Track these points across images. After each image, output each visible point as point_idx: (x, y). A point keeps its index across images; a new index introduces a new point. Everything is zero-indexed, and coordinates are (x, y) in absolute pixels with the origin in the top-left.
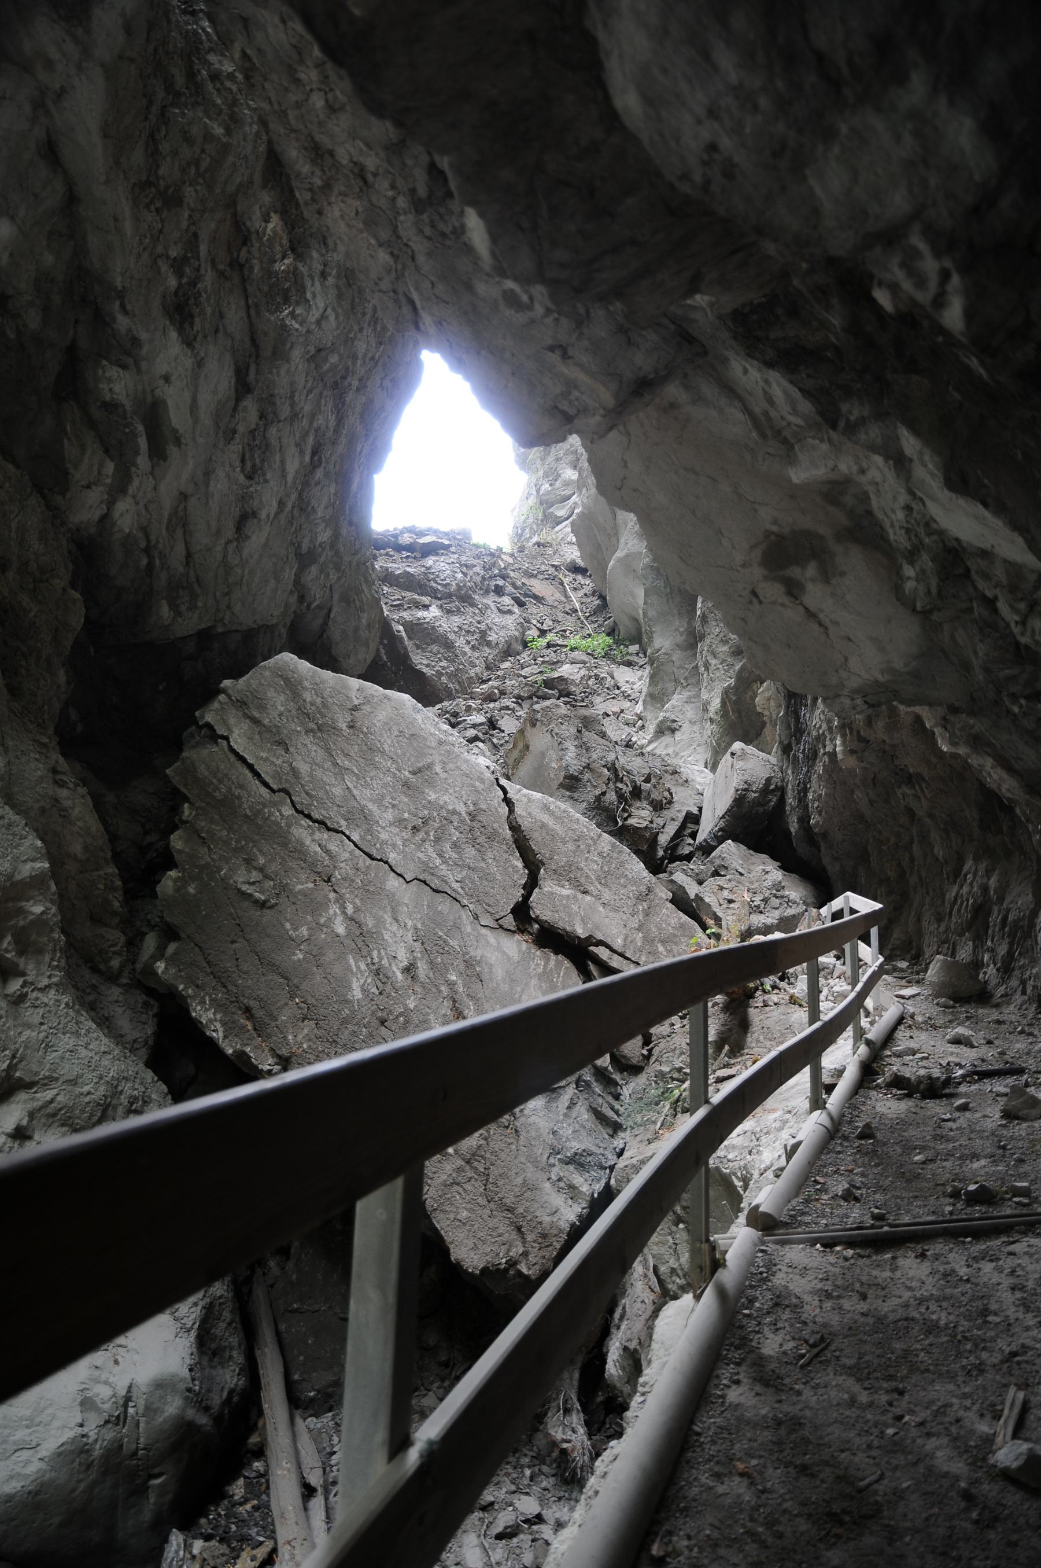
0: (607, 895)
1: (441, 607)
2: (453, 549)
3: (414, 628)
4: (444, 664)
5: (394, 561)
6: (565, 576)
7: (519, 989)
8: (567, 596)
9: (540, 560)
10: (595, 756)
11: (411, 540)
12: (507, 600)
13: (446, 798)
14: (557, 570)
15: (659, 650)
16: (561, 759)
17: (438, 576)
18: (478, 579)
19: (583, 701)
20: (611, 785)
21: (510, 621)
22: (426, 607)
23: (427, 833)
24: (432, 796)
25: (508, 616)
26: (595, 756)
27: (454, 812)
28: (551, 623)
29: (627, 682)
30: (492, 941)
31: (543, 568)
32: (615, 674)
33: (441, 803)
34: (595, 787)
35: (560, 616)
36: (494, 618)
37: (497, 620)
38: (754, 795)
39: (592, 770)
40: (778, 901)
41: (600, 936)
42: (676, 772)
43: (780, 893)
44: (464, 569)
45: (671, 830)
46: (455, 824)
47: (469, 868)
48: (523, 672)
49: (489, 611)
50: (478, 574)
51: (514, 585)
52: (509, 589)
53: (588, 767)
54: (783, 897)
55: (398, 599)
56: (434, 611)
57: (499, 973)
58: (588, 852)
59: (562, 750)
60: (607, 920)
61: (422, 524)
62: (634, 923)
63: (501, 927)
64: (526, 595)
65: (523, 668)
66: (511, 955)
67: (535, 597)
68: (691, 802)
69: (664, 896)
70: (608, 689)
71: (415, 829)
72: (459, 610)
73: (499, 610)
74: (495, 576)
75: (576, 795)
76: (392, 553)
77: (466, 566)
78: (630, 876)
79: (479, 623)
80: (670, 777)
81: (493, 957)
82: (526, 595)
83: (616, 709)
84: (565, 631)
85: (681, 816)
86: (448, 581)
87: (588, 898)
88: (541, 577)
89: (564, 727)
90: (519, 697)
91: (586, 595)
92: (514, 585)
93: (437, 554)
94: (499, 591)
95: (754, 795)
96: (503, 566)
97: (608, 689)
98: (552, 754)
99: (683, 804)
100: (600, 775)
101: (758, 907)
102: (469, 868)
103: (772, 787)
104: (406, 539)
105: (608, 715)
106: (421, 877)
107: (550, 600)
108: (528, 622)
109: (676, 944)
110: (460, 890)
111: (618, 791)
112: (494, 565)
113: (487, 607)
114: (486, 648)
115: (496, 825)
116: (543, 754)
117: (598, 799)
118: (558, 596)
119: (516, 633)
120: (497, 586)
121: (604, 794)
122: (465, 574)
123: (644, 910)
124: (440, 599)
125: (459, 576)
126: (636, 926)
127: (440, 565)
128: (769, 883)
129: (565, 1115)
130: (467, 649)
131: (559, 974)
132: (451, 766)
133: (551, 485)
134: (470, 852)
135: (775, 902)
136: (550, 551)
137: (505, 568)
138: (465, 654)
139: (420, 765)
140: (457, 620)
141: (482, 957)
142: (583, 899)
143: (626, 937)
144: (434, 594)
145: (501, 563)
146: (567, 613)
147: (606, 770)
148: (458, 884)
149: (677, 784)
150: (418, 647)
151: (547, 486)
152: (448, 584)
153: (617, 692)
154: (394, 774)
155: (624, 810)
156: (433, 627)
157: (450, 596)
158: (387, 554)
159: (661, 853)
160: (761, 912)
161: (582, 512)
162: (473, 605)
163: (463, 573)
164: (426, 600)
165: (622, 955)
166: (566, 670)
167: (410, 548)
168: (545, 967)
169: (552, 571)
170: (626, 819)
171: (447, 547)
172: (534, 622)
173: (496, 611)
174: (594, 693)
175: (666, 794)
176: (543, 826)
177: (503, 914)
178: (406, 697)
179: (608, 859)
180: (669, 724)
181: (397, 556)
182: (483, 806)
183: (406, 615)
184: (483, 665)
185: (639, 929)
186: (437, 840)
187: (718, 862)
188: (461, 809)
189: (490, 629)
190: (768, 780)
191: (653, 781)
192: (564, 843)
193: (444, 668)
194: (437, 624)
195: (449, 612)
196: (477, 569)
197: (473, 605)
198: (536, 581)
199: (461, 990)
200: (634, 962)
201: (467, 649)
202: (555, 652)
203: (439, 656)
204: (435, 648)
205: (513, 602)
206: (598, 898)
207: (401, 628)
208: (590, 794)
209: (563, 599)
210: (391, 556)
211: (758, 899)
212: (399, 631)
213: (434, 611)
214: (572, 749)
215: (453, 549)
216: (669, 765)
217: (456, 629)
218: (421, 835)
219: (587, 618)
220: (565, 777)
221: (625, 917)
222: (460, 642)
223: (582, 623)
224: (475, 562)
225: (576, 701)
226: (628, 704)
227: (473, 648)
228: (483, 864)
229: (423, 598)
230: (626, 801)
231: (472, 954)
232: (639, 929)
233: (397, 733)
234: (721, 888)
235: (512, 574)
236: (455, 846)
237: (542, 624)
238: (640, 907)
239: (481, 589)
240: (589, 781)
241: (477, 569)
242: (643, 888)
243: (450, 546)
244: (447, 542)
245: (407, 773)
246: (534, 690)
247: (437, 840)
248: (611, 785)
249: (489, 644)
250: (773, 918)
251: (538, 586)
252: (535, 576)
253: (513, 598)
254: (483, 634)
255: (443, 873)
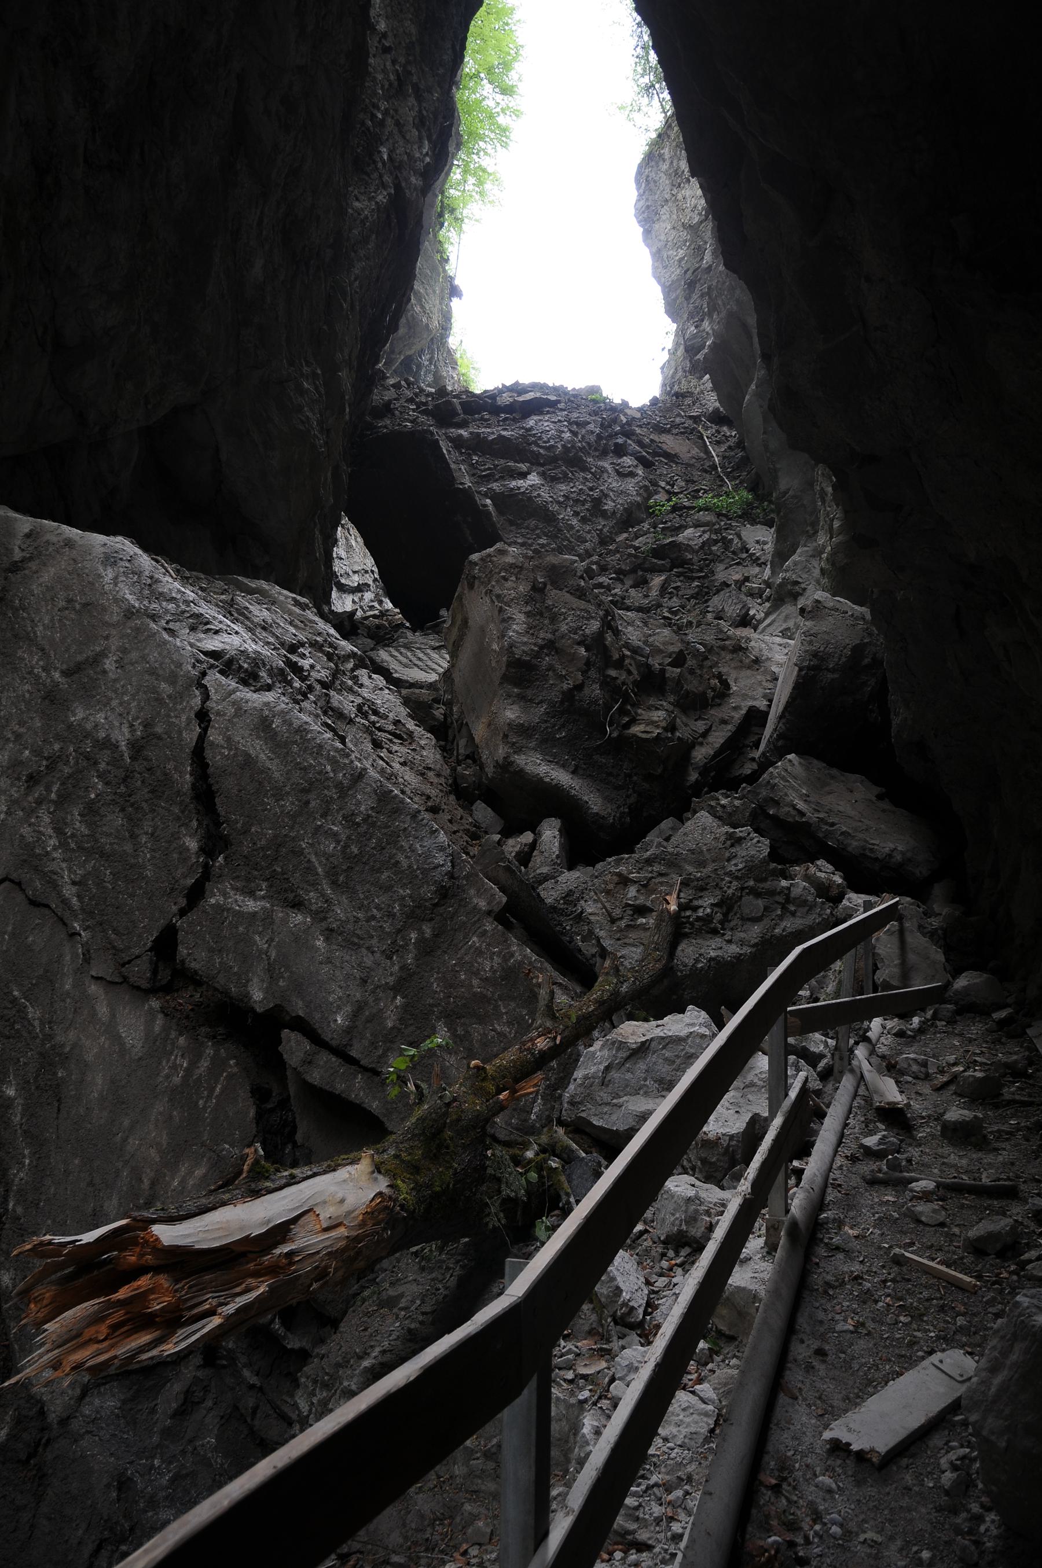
0: (341, 911)
1: (543, 475)
2: (561, 406)
3: (507, 501)
4: (543, 541)
5: (489, 426)
6: (706, 429)
7: (126, 1123)
8: (707, 452)
9: (676, 411)
10: (564, 628)
11: (511, 400)
12: (628, 461)
13: (100, 717)
14: (695, 422)
15: (786, 493)
16: (503, 636)
17: (540, 438)
18: (592, 438)
19: (701, 570)
20: (593, 673)
21: (630, 486)
22: (523, 475)
23: (48, 789)
24: (79, 714)
25: (629, 480)
26: (564, 628)
27: (108, 744)
28: (683, 484)
29: (758, 542)
30: (103, 1010)
31: (678, 420)
32: (743, 534)
33: (89, 726)
34: (562, 678)
35: (696, 474)
36: (614, 483)
37: (614, 484)
38: (830, 676)
39: (558, 651)
40: (760, 903)
41: (299, 1008)
42: (741, 649)
43: (767, 885)
44: (575, 428)
45: (718, 738)
46: (102, 766)
47: (102, 854)
48: (636, 543)
49: (605, 475)
50: (592, 432)
51: (640, 443)
52: (634, 446)
53: (550, 646)
54: (772, 893)
55: (489, 469)
56: (534, 479)
57: (98, 1082)
58: (324, 815)
59: (504, 620)
60: (325, 969)
61: (526, 380)
62: (389, 973)
63: (125, 979)
64: (655, 454)
65: (637, 538)
66: (129, 1041)
67: (667, 455)
68: (760, 691)
69: (483, 904)
70: (734, 553)
71: (33, 780)
72: (566, 475)
73: (618, 473)
74: (616, 434)
75: (529, 693)
76: (486, 417)
77: (577, 424)
78: (405, 863)
79: (591, 489)
80: (729, 656)
81: (93, 1048)
82: (655, 454)
83: (737, 577)
84: (698, 491)
85: (738, 716)
86: (552, 442)
87: (298, 918)
88: (675, 431)
89: (509, 584)
90: (620, 572)
91: (730, 447)
92: (640, 443)
93: (541, 413)
94: (620, 451)
95: (830, 676)
96: (624, 420)
97: (734, 553)
98: (493, 629)
99: (745, 697)
100: (574, 657)
101: (708, 919)
102: (102, 854)
103: (866, 661)
104: (506, 399)
105: (728, 586)
106: (14, 876)
107: (685, 456)
108: (655, 484)
109: (481, 1020)
110: (75, 900)
111: (607, 683)
112: (615, 421)
113: (603, 470)
114: (601, 520)
115: (170, 766)
116: (483, 630)
117: (568, 696)
118: (695, 451)
119: (638, 499)
120: (616, 444)
121: (579, 687)
122: (574, 434)
123: (421, 940)
124: (542, 465)
125: (567, 435)
126: (391, 980)
127: (541, 425)
128: (736, 866)
129: (166, 1432)
130: (574, 522)
131: (212, 1090)
132: (134, 655)
133: (696, 327)
134: (116, 820)
135: (754, 905)
136: (688, 401)
137: (628, 423)
138: (572, 527)
139: (80, 658)
140: (563, 488)
141: (74, 1046)
142: (285, 921)
143: (359, 1008)
144: (535, 461)
145: (622, 417)
146: (706, 471)
147: (582, 651)
148: (74, 889)
149: (742, 666)
150: (511, 523)
151: (693, 328)
152: (552, 446)
153: (744, 555)
154: (38, 677)
155: (622, 711)
156: (530, 498)
157: (553, 460)
158: (482, 419)
159: (693, 776)
160: (715, 932)
161: (713, 342)
162: (585, 469)
163: (571, 432)
164: (523, 467)
165: (341, 1053)
166: (690, 535)
167: (510, 408)
168: (189, 1071)
169: (689, 423)
170: (627, 726)
171: (553, 404)
172: (663, 484)
173: (613, 473)
174: (717, 559)
175: (715, 682)
176: (248, 762)
177: (137, 951)
178: (120, 538)
179: (363, 829)
180: (789, 587)
181: (493, 420)
182: (159, 729)
183: (495, 486)
184: (596, 540)
185: (397, 989)
186: (63, 799)
187: (764, 793)
188: (122, 736)
189: (606, 496)
190: (858, 650)
191: (690, 662)
192: (278, 795)
193: (543, 546)
194: (535, 494)
195: (554, 479)
196: (591, 427)
197: (585, 469)
198: (670, 437)
199: (17, 1119)
200: (366, 1069)
201: (574, 522)
202: (680, 516)
203: (538, 531)
204: (533, 523)
205: (635, 463)
206: (320, 916)
207: (488, 501)
208: (555, 689)
209: (702, 455)
210: (487, 420)
211: (706, 903)
212: (485, 506)
213: (534, 479)
214: (521, 617)
215: (561, 406)
216: (729, 638)
217: (561, 499)
218: (39, 791)
219: (728, 475)
220: (509, 664)
221: (368, 961)
222: (566, 514)
223: (722, 480)
224: (588, 419)
225: (692, 571)
226: (757, 569)
227: (584, 520)
228: (128, 847)
229: (521, 465)
230: (626, 699)
231: (60, 1039)
232: (397, 989)
233: (62, 604)
234: (624, 881)
235: (638, 431)
236: (91, 811)
237: (673, 486)
238: (413, 936)
239: (596, 450)
240: (551, 667)
241: (591, 427)
242: (428, 892)
243: (559, 402)
244: (553, 398)
245: (57, 675)
246: (639, 561)
247: (63, 799)
248: (593, 673)
249: (604, 514)
250: (742, 943)
251: (670, 443)
252: (668, 431)
253: (636, 459)
254: (597, 503)
255: (53, 866)
